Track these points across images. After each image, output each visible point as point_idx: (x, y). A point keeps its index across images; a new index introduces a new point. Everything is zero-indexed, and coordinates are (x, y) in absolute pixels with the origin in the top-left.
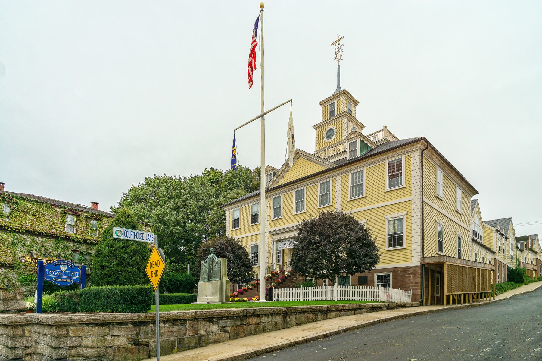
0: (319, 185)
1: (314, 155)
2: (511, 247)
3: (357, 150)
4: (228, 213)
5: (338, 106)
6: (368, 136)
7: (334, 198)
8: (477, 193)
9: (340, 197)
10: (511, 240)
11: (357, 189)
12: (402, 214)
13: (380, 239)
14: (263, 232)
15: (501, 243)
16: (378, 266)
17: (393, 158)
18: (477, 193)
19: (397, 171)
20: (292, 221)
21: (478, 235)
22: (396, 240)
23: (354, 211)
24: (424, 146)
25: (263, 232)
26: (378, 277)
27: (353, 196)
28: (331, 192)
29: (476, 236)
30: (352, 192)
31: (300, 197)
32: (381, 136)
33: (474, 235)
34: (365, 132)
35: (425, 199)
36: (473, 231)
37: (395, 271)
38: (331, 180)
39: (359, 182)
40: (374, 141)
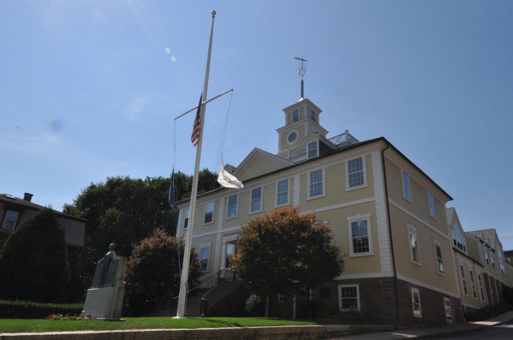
0: (277, 184)
1: (276, 155)
2: (501, 261)
3: (316, 150)
4: (181, 211)
5: (303, 114)
6: (330, 139)
7: (292, 196)
8: (451, 199)
9: (297, 199)
10: (500, 255)
11: (316, 189)
12: (366, 216)
13: (342, 240)
14: (207, 238)
15: (489, 255)
16: (342, 277)
17: (353, 155)
18: (451, 199)
19: (358, 170)
20: (236, 228)
21: (460, 246)
22: (361, 245)
23: (317, 210)
24: (384, 144)
25: (207, 238)
26: (343, 289)
27: (312, 195)
28: (289, 190)
29: (459, 247)
30: (312, 191)
31: (283, 186)
32: (343, 139)
33: (455, 244)
34: (328, 137)
35: (390, 200)
36: (455, 241)
37: (363, 282)
38: (289, 178)
39: (318, 180)
40: (336, 144)
